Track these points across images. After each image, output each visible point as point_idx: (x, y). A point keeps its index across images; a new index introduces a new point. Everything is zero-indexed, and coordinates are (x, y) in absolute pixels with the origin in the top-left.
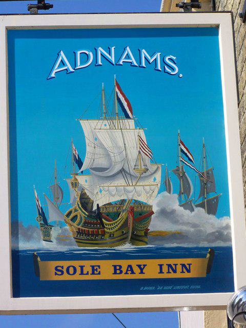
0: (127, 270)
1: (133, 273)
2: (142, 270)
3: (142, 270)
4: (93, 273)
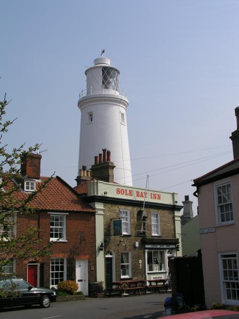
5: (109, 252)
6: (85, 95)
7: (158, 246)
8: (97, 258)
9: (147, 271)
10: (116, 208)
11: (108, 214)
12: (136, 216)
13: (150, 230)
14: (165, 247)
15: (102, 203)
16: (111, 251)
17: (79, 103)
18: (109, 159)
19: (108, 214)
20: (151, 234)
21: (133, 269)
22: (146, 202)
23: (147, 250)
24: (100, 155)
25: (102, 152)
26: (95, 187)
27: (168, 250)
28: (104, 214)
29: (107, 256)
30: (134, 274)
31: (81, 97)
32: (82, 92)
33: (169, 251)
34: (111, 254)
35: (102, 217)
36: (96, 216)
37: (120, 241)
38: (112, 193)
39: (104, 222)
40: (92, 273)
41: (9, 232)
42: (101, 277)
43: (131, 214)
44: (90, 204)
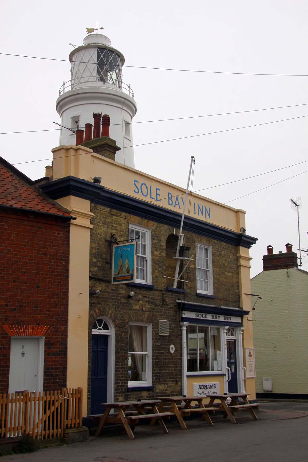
0: (215, 317)
1: (217, 319)
2: (219, 318)
3: (219, 318)
4: (205, 317)
5: (100, 321)
6: (68, 89)
7: (209, 317)
8: (135, 169)
9: (186, 373)
10: (121, 220)
11: (102, 230)
12: (164, 244)
13: (193, 280)
14: (222, 318)
15: (89, 202)
16: (105, 319)
17: (58, 104)
18: (106, 132)
19: (102, 230)
20: (195, 288)
21: (155, 364)
22: (186, 218)
23: (186, 324)
24: (88, 126)
25: (92, 121)
26: (74, 212)
27: (227, 327)
28: (91, 226)
29: (95, 332)
30: (156, 377)
31: (62, 94)
32: (64, 84)
33: (229, 330)
34: (106, 327)
35: (87, 233)
36: (72, 229)
37: (129, 297)
38: (113, 182)
39: (91, 248)
40: (55, 373)
41: (101, 302)
42: (78, 374)
43: (153, 239)
44: (58, 201)
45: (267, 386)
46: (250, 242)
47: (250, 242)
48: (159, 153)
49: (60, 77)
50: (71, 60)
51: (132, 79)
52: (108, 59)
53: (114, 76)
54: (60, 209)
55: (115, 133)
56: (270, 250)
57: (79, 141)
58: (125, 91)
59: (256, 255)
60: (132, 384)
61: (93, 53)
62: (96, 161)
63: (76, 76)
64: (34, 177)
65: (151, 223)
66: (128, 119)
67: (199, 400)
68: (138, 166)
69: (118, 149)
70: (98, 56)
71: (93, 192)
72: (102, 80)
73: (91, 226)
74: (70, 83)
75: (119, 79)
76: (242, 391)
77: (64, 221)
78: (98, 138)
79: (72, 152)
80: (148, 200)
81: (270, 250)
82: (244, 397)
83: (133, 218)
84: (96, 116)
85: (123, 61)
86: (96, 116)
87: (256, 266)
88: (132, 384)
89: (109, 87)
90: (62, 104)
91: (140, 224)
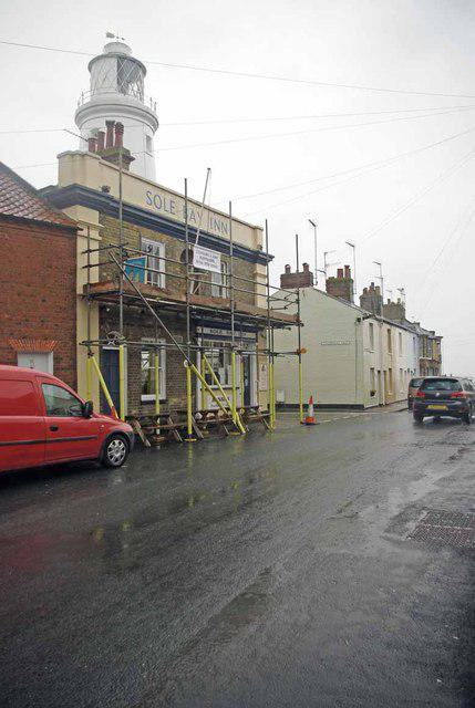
6: (87, 100)
18: (119, 141)
28: (100, 238)
30: (169, 390)
38: (135, 197)
44: (64, 211)
45: (281, 398)
46: (265, 259)
47: (265, 259)
48: (182, 162)
49: (77, 86)
50: (90, 69)
51: (156, 89)
52: (128, 68)
53: (136, 88)
54: (66, 219)
55: (131, 141)
56: (288, 268)
57: (92, 148)
58: (147, 104)
59: (275, 272)
60: (145, 398)
61: (114, 62)
62: (105, 168)
63: (95, 87)
64: (38, 185)
65: (165, 237)
66: (150, 134)
67: (215, 412)
68: (160, 181)
69: (133, 159)
70: (119, 66)
71: (104, 204)
72: (123, 91)
73: (100, 238)
74: (89, 94)
75: (141, 92)
76: (254, 402)
77: (72, 231)
78: (109, 147)
79: (78, 158)
80: (162, 212)
81: (288, 268)
82: (257, 408)
83: (146, 231)
84: (109, 124)
85: (145, 72)
86: (109, 124)
87: (275, 281)
88: (145, 398)
89: (130, 98)
90: (80, 117)
91: (153, 238)
